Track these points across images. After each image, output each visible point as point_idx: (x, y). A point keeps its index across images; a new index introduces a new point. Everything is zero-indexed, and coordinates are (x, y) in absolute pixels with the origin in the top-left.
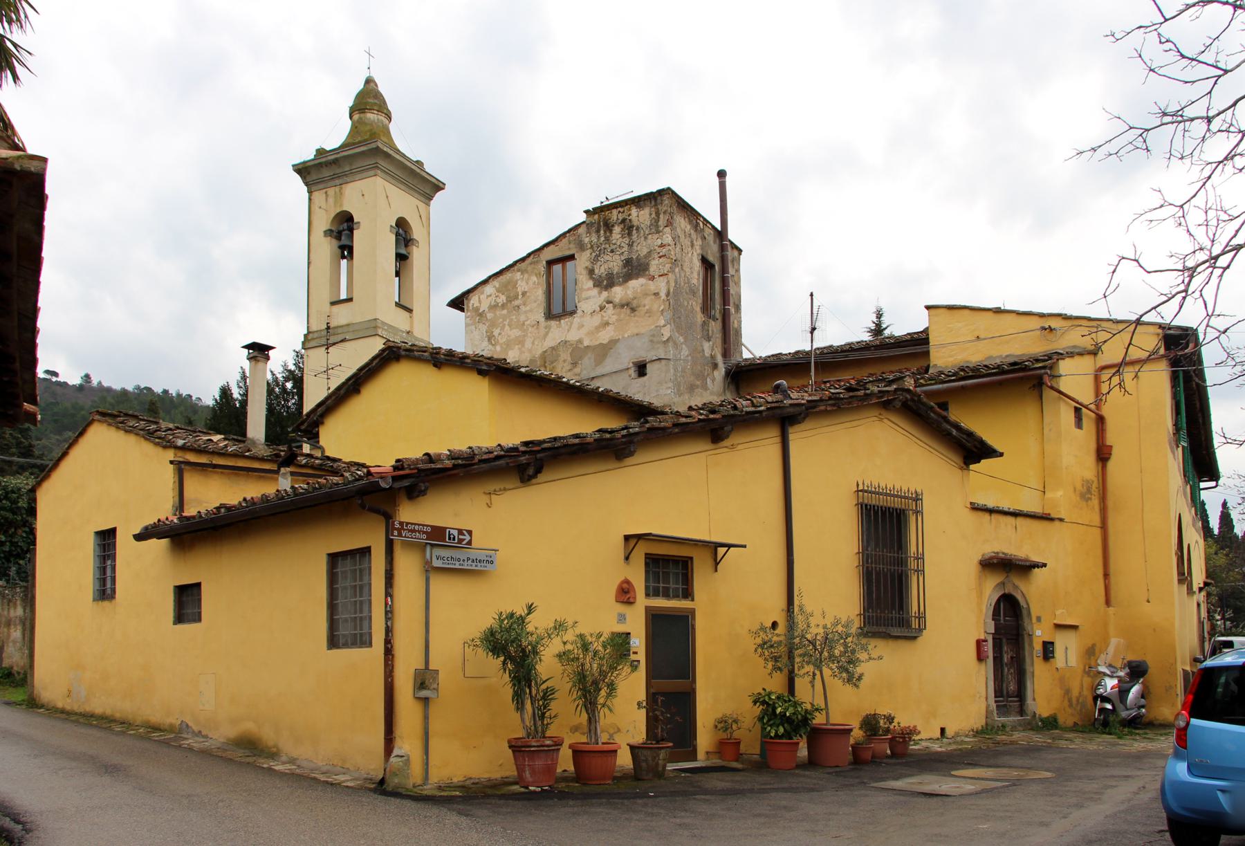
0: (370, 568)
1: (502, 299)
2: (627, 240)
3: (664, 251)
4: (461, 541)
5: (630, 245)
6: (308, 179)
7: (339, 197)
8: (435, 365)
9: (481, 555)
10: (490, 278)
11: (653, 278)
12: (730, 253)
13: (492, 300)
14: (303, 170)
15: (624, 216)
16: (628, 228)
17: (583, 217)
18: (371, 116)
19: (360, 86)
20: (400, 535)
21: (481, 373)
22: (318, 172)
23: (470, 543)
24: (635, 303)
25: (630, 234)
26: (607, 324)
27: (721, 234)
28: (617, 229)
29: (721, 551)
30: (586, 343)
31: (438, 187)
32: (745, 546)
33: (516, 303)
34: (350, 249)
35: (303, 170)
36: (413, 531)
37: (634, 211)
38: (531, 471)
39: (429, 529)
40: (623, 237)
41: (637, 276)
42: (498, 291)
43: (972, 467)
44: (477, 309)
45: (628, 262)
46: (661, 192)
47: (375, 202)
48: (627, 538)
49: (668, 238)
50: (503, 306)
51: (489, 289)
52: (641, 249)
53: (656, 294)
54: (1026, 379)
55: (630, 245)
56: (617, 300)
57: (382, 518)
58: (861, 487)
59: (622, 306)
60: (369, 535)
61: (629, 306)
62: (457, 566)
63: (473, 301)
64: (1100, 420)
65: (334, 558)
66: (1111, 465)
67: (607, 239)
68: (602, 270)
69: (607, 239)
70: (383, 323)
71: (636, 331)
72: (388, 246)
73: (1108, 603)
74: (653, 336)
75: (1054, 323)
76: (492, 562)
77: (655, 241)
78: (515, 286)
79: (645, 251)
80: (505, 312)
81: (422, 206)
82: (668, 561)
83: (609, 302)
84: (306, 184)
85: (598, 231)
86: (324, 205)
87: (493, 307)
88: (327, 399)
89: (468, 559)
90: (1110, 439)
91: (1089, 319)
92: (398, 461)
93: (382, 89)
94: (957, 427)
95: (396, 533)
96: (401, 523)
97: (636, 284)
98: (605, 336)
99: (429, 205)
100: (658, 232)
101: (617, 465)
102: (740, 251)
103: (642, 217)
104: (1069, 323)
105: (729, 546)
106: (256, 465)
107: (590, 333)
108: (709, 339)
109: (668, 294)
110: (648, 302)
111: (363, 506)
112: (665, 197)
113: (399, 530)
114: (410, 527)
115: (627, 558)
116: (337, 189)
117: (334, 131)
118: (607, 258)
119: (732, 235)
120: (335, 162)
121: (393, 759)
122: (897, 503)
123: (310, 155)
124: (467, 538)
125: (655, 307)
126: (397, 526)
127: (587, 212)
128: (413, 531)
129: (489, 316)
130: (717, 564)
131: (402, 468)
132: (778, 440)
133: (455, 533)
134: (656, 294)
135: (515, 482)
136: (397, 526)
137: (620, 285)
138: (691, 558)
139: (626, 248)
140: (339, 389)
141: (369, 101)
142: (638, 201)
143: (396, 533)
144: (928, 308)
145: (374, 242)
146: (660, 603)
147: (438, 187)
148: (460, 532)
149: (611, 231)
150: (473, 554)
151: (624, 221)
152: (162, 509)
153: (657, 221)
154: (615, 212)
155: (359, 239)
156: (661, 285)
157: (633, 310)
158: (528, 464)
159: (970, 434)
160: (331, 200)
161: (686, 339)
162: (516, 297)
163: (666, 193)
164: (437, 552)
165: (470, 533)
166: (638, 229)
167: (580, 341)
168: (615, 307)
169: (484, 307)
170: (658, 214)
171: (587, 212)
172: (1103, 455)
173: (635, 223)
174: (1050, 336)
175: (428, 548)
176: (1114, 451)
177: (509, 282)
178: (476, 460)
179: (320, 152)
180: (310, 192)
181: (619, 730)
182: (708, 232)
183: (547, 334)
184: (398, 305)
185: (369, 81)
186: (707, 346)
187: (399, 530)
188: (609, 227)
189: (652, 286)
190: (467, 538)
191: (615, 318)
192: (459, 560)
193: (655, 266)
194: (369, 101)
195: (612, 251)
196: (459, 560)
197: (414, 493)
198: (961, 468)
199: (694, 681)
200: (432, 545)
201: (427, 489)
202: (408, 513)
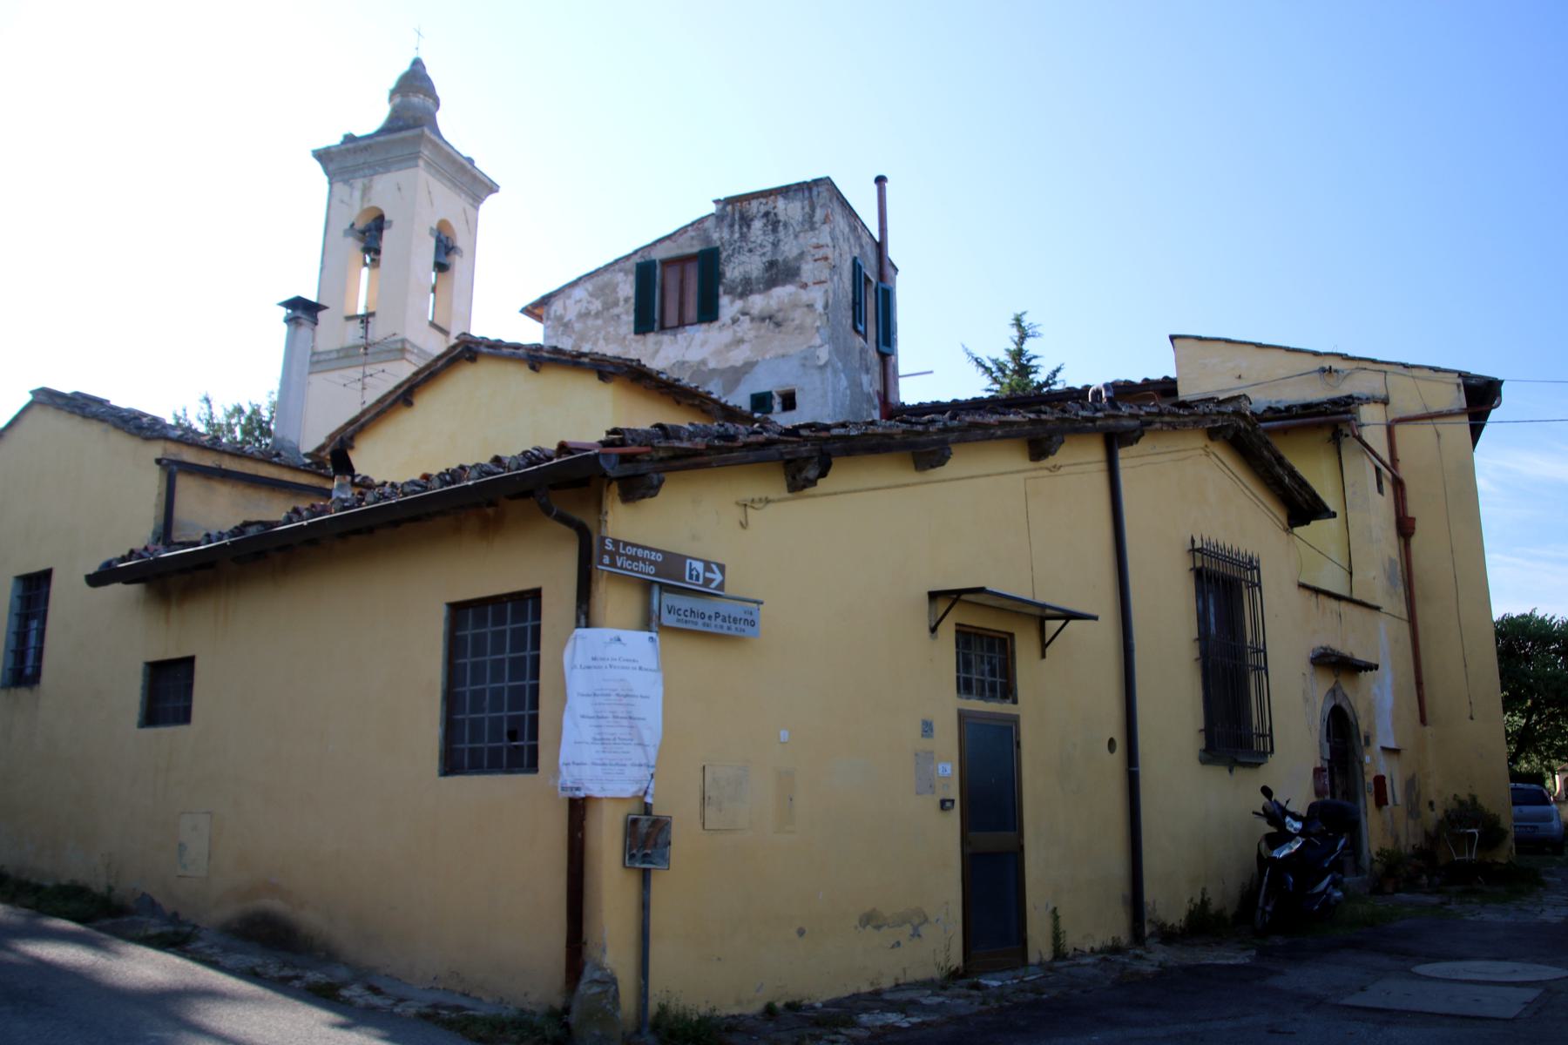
0: (537, 631)
1: (597, 305)
2: (771, 238)
3: (820, 253)
4: (708, 581)
5: (775, 245)
6: (331, 168)
7: (366, 191)
8: (533, 368)
9: (737, 610)
10: (580, 279)
11: (805, 286)
12: (889, 271)
13: (582, 307)
14: (324, 156)
15: (769, 207)
16: (773, 222)
17: (712, 209)
18: (417, 100)
19: (405, 67)
20: (613, 564)
21: (604, 376)
22: (344, 161)
23: (721, 586)
24: (780, 316)
25: (775, 230)
26: (740, 341)
27: (881, 247)
28: (757, 225)
29: (1052, 626)
30: (712, 365)
31: (492, 188)
32: (1095, 618)
33: (616, 311)
34: (378, 252)
35: (324, 156)
36: (634, 558)
37: (781, 203)
38: (811, 473)
39: (659, 557)
40: (764, 233)
41: (784, 283)
42: (591, 295)
43: (1297, 530)
44: (560, 319)
45: (772, 264)
46: (816, 182)
47: (416, 201)
48: (934, 596)
49: (825, 238)
50: (597, 315)
51: (579, 293)
52: (789, 249)
53: (810, 306)
54: (1331, 420)
55: (775, 245)
56: (755, 311)
57: (572, 533)
58: (1198, 545)
59: (763, 319)
60: (535, 563)
61: (772, 320)
62: (700, 627)
63: (557, 307)
64: (1398, 484)
65: (458, 611)
66: (1415, 541)
67: (743, 236)
68: (736, 273)
69: (743, 236)
70: (414, 346)
71: (781, 352)
72: (426, 252)
73: (1423, 721)
74: (805, 358)
75: (1337, 364)
76: (753, 623)
77: (810, 239)
78: (614, 290)
79: (795, 252)
80: (599, 322)
81: (468, 207)
82: (981, 636)
83: (744, 314)
84: (327, 173)
85: (732, 226)
86: (346, 199)
87: (584, 316)
88: (363, 414)
89: (717, 615)
90: (1412, 510)
91: (1374, 361)
92: (615, 431)
93: (430, 72)
94: (1293, 474)
95: (606, 560)
96: (616, 542)
97: (782, 293)
98: (738, 357)
99: (477, 209)
100: (812, 228)
101: (913, 476)
102: (896, 270)
103: (790, 210)
104: (1354, 364)
105: (1069, 616)
106: (287, 476)
107: (718, 353)
108: (867, 371)
109: (826, 306)
110: (798, 316)
111: (547, 510)
112: (822, 189)
113: (612, 555)
114: (631, 551)
115: (933, 630)
116: (366, 181)
117: (371, 116)
118: (743, 258)
119: (893, 253)
120: (365, 149)
121: (582, 987)
122: (1230, 571)
123: (335, 139)
124: (718, 577)
125: (809, 321)
126: (610, 547)
127: (717, 202)
128: (634, 558)
129: (578, 326)
130: (1044, 645)
131: (623, 443)
132: (1103, 466)
133: (699, 566)
134: (810, 306)
135: (775, 487)
136: (610, 547)
137: (760, 292)
138: (1012, 635)
139: (769, 248)
140: (380, 401)
141: (415, 86)
142: (784, 191)
143: (606, 560)
144: (1172, 338)
145: (410, 246)
146: (976, 705)
147: (492, 188)
148: (708, 566)
149: (749, 227)
150: (724, 607)
151: (767, 214)
152: (132, 530)
153: (812, 216)
154: (754, 203)
155: (388, 239)
156: (816, 296)
157: (778, 325)
158: (808, 459)
159: (1303, 484)
160: (357, 194)
161: (845, 366)
162: (616, 304)
163: (826, 183)
164: (670, 599)
165: (722, 568)
166: (785, 225)
167: (704, 362)
168: (752, 320)
169: (571, 315)
170: (813, 209)
171: (717, 202)
172: (1405, 527)
173: (782, 218)
174: (1332, 380)
175: (656, 590)
176: (1418, 526)
177: (606, 285)
178: (739, 443)
179: (349, 138)
180: (331, 183)
181: (926, 920)
182: (865, 239)
183: (657, 351)
184: (433, 324)
185: (417, 63)
186: (865, 379)
187: (612, 555)
188: (746, 221)
189: (805, 296)
190: (718, 577)
191: (751, 334)
192: (702, 616)
193: (808, 270)
194: (415, 86)
195: (750, 251)
196: (702, 616)
197: (637, 487)
198: (1286, 530)
199: (1021, 835)
200: (661, 585)
201: (661, 482)
202: (623, 522)
